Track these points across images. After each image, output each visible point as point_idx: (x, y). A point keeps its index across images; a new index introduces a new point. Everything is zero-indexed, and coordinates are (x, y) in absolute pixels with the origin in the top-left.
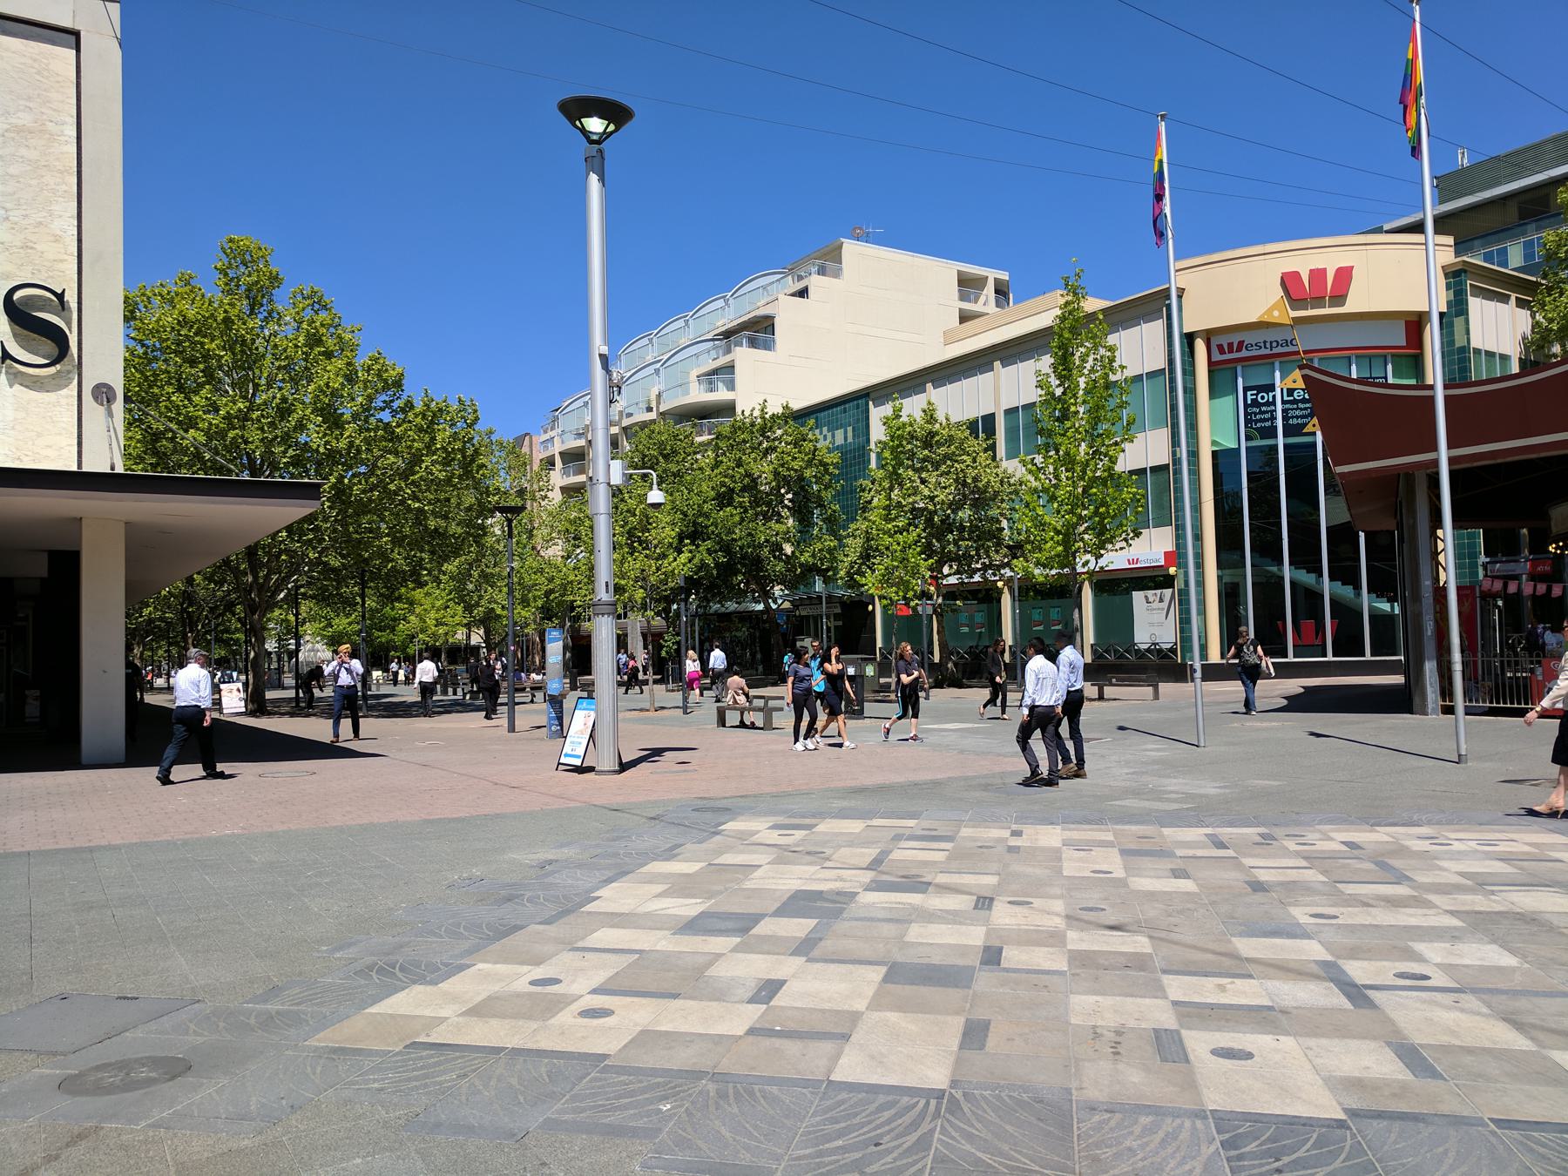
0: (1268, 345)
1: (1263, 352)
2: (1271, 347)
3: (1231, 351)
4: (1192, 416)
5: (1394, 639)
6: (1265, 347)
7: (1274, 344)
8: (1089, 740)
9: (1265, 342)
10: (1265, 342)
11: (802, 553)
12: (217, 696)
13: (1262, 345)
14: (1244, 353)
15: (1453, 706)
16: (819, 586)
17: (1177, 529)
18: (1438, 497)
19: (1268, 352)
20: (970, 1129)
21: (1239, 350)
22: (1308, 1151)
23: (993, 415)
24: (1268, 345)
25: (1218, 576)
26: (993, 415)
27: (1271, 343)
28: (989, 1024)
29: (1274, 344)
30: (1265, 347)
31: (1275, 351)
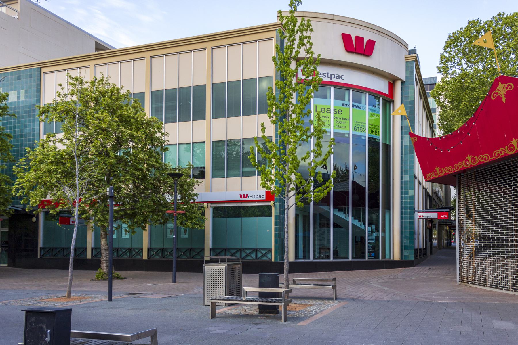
0: (329, 76)
2: (256, 198)
3: (244, 197)
5: (204, 111)
6: (328, 77)
7: (257, 197)
8: (114, 289)
9: (254, 195)
10: (254, 195)
11: (264, 167)
13: (253, 196)
14: (248, 199)
16: (96, 134)
18: (345, 259)
21: (246, 197)
22: (434, 199)
24: (329, 76)
27: (331, 75)
28: (156, 330)
29: (257, 197)
30: (328, 77)
31: (257, 199)
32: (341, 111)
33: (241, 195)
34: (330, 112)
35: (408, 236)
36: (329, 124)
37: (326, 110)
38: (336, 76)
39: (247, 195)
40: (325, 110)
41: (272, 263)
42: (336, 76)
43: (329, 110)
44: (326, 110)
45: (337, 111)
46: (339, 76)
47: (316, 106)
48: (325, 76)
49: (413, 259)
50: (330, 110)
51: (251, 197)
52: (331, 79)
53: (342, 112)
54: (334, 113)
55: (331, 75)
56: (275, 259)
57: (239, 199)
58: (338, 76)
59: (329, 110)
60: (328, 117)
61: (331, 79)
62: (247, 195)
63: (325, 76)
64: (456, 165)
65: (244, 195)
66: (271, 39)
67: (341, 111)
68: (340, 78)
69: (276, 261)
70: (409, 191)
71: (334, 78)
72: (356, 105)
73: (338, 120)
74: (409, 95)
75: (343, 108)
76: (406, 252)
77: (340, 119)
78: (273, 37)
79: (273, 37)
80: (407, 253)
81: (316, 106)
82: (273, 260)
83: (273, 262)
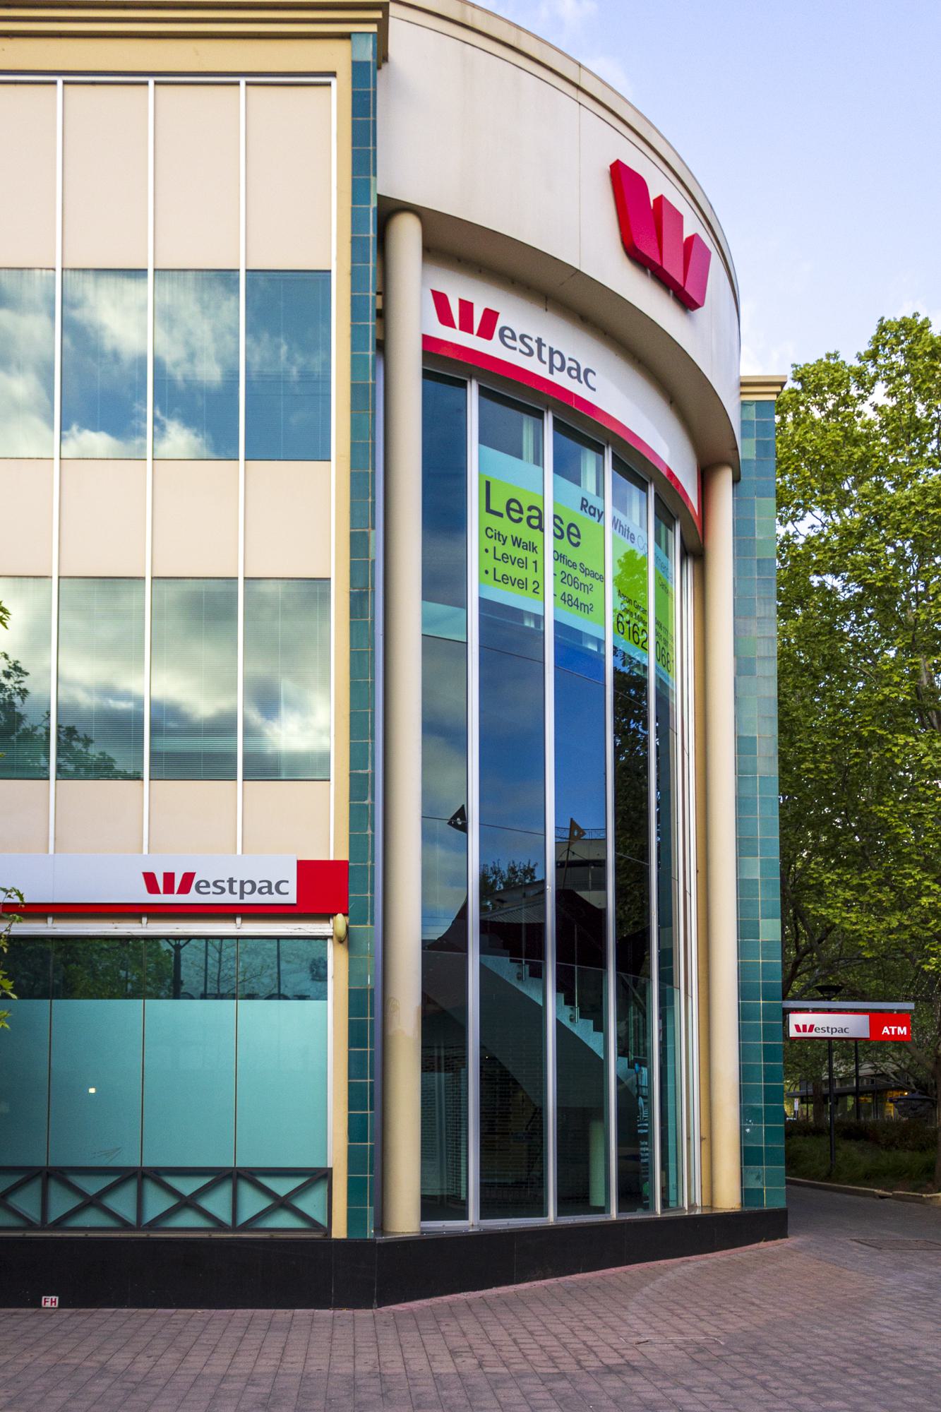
0: (236, 887)
1: (227, 898)
2: (242, 892)
3: (169, 889)
4: (665, 1194)
6: (231, 891)
7: (248, 888)
9: (231, 881)
10: (231, 881)
12: (597, 577)
13: (226, 886)
14: (192, 897)
15: (540, 964)
17: (367, 184)
19: (235, 899)
20: (632, 1034)
21: (185, 888)
23: (786, 1180)
24: (236, 887)
25: (352, 535)
26: (786, 1180)
27: (242, 883)
29: (248, 888)
30: (231, 891)
31: (248, 899)
32: (575, 532)
33: (150, 878)
34: (541, 527)
35: (760, 1110)
36: (538, 577)
37: (526, 513)
38: (258, 886)
39: (188, 878)
40: (521, 511)
41: (328, 1244)
42: (258, 886)
43: (535, 513)
44: (526, 513)
45: (565, 528)
46: (270, 883)
47: (488, 484)
48: (223, 890)
49: (781, 1203)
50: (540, 517)
51: (212, 889)
52: (242, 897)
53: (578, 536)
54: (555, 535)
55: (242, 883)
56: (354, 1218)
57: (141, 895)
58: (266, 884)
59: (535, 513)
60: (534, 549)
61: (242, 897)
62: (188, 878)
63: (223, 890)
64: (441, 1225)
65: (169, 877)
66: (319, 78)
67: (575, 532)
68: (273, 890)
69: (357, 1236)
70: (761, 922)
71: (252, 892)
72: (623, 523)
73: (568, 570)
74: (758, 536)
75: (585, 522)
76: (754, 1176)
77: (574, 565)
78: (333, 74)
79: (333, 74)
80: (758, 1178)
81: (488, 484)
82: (339, 1231)
83: (338, 1241)
